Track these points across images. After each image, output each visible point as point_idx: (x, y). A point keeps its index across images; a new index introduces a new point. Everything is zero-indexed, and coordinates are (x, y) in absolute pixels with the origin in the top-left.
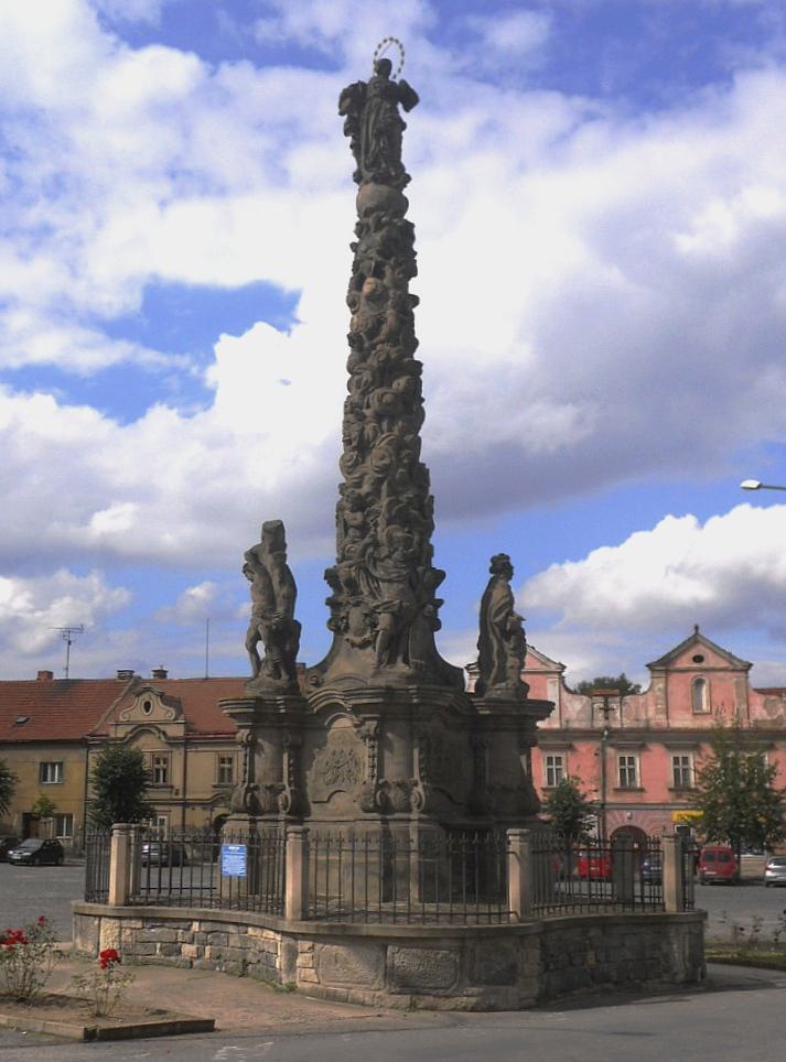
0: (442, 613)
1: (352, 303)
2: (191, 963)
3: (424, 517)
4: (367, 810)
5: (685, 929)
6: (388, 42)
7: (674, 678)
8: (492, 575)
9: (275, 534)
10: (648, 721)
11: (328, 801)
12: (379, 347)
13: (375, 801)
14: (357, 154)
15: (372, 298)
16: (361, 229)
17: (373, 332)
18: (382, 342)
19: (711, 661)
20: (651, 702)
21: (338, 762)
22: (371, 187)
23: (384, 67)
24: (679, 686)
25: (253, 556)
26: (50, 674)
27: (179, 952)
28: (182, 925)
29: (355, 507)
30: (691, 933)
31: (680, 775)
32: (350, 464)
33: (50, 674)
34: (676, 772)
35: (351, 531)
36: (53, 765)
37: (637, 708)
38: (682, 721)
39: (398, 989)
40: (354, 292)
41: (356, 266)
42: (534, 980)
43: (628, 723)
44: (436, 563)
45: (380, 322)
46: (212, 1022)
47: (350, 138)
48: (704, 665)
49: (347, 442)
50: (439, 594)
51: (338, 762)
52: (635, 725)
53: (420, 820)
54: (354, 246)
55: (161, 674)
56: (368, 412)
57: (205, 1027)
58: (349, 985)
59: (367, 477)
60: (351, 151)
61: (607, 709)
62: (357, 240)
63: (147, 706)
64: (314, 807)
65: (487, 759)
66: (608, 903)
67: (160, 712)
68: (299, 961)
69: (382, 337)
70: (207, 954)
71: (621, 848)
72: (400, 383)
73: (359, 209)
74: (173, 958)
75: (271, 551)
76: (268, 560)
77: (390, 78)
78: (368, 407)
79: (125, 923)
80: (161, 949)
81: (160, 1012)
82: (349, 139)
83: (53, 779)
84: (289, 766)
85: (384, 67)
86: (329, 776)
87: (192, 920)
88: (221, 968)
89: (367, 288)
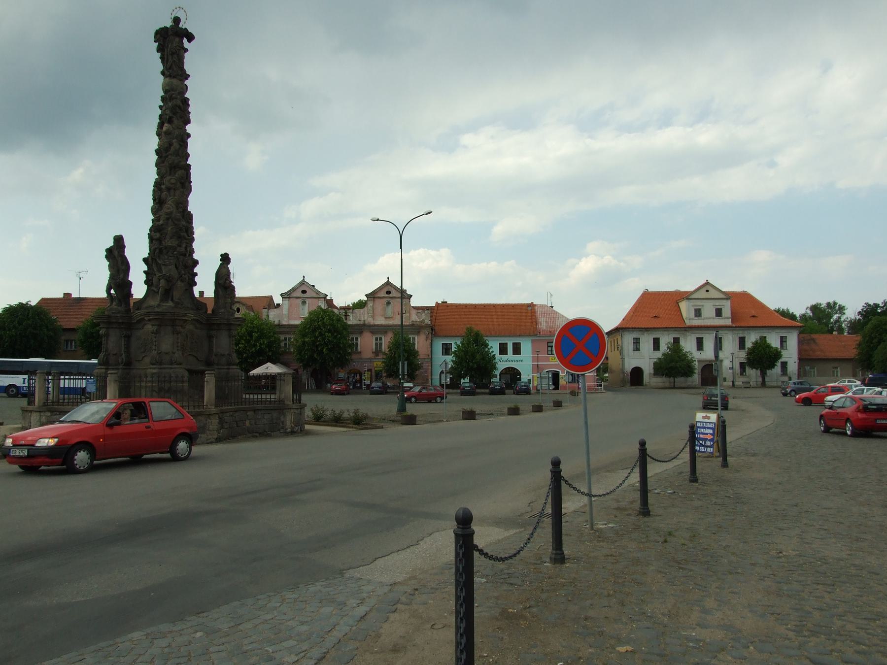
0: (197, 279)
4: (153, 364)
7: (378, 301)
9: (119, 241)
14: (163, 62)
15: (168, 133)
16: (163, 99)
17: (167, 149)
22: (167, 79)
23: (177, 20)
31: (379, 345)
34: (376, 344)
36: (71, 341)
38: (380, 321)
41: (161, 117)
44: (195, 256)
45: (171, 145)
48: (391, 295)
49: (154, 200)
50: (196, 270)
54: (161, 107)
56: (163, 187)
72: (180, 173)
76: (116, 253)
85: (177, 20)
89: (164, 129)
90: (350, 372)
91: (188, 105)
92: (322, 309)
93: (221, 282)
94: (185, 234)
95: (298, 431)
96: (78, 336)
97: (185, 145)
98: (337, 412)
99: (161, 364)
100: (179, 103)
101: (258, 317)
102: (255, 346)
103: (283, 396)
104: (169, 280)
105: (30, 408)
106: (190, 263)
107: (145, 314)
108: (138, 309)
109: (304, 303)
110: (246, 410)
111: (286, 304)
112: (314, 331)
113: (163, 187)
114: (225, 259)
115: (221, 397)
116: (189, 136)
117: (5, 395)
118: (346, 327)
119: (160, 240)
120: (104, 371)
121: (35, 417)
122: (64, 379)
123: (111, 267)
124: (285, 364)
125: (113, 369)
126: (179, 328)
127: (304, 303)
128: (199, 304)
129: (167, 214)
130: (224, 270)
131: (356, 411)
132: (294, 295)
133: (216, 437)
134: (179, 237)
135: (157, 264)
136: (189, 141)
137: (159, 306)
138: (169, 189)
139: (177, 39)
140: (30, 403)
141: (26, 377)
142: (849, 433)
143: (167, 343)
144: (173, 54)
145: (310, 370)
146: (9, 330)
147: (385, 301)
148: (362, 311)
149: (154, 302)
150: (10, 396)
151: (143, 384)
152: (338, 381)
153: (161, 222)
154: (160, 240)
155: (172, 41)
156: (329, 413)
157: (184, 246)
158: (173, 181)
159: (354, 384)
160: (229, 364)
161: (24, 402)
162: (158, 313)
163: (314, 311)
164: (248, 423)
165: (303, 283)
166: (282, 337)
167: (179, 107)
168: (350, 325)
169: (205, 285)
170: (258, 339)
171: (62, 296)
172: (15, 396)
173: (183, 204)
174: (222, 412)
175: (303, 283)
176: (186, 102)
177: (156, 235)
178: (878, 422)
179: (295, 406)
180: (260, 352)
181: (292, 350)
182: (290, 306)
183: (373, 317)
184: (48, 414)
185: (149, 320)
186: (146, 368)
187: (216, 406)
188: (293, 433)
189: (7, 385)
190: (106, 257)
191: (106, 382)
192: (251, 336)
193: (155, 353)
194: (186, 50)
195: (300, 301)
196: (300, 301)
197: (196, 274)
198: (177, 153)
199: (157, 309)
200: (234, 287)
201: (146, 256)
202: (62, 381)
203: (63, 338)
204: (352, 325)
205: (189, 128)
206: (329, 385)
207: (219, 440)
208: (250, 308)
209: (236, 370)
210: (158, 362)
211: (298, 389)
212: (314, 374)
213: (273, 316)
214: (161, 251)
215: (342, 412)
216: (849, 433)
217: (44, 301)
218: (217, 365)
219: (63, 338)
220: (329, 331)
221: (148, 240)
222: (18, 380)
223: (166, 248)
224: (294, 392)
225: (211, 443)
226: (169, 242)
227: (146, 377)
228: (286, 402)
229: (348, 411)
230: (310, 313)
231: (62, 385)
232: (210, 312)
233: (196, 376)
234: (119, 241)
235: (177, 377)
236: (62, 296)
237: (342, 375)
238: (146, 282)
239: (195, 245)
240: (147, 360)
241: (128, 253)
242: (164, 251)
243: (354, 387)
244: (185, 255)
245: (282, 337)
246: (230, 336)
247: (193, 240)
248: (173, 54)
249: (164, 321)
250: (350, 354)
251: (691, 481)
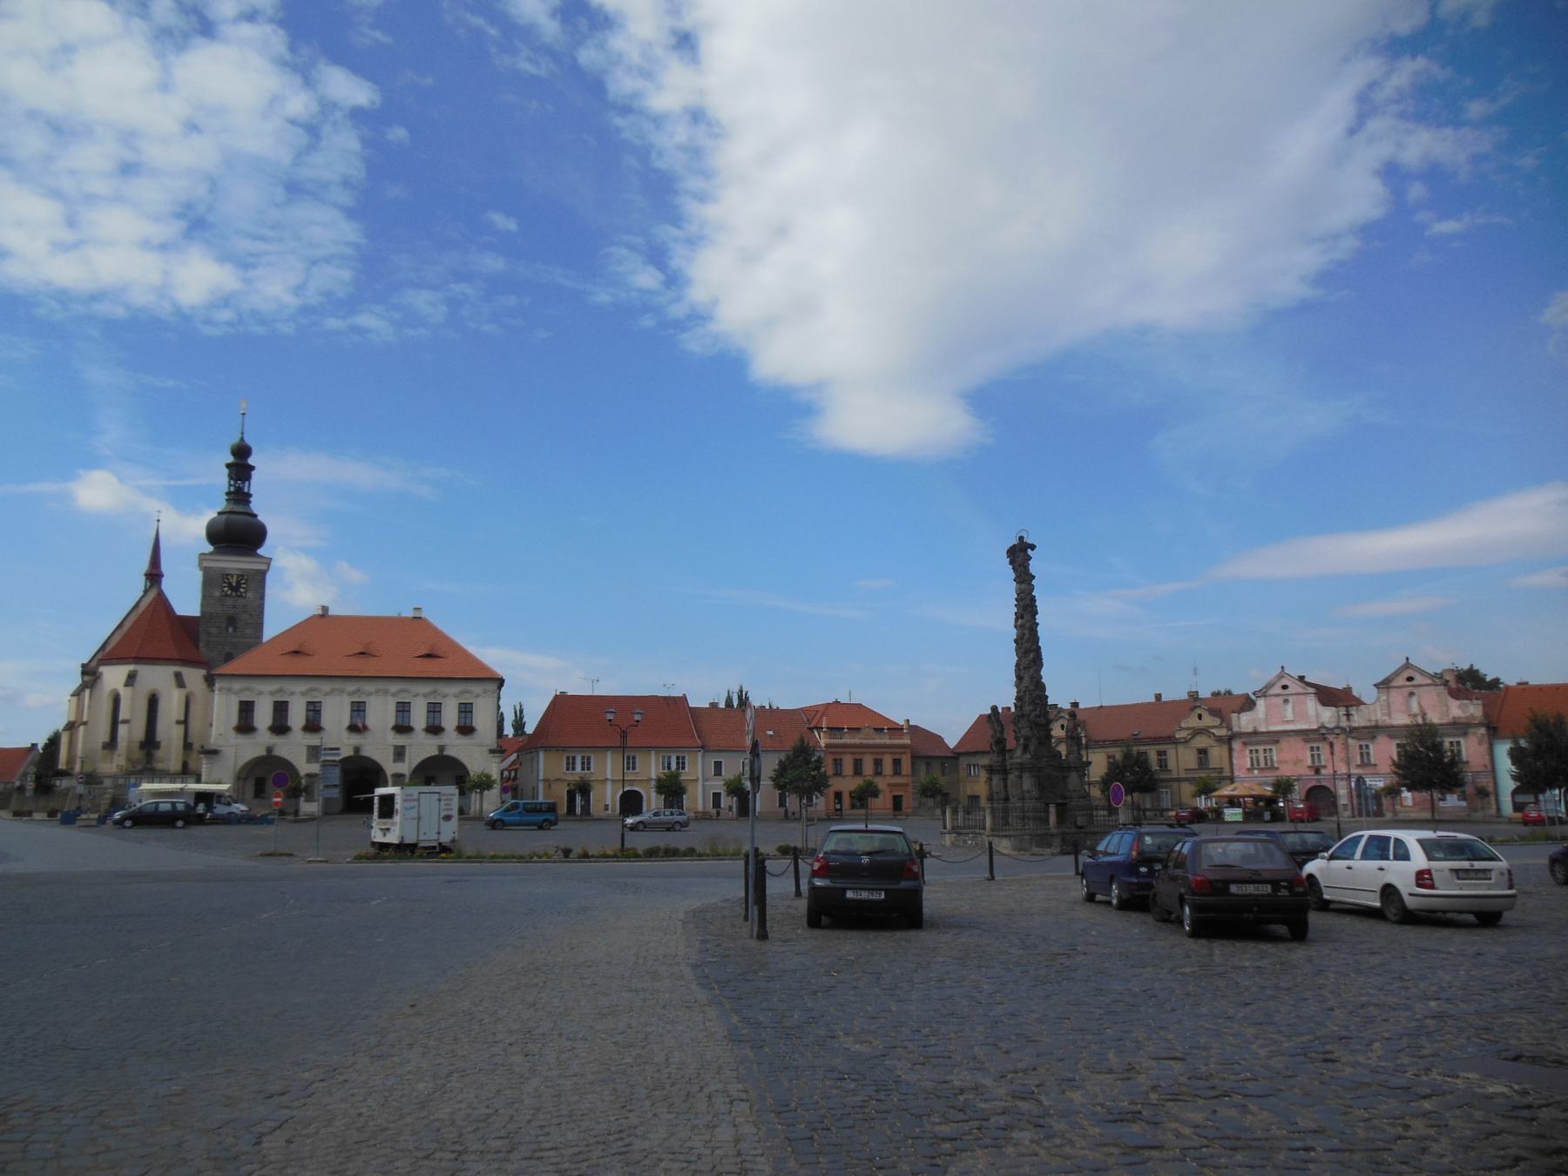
7: (1394, 693)
19: (1419, 679)
23: (1021, 538)
24: (1397, 698)
29: (46, 747)
43: (1363, 723)
55: (1075, 705)
61: (1348, 715)
63: (1200, 717)
66: (264, 1134)
67: (1208, 720)
72: (1032, 656)
85: (1021, 538)
142: (1115, 901)
147: (1406, 691)
155: (1019, 554)
178: (850, 895)
183: (1389, 715)
195: (1280, 700)
196: (1280, 700)
216: (1115, 901)
251: (1299, 933)
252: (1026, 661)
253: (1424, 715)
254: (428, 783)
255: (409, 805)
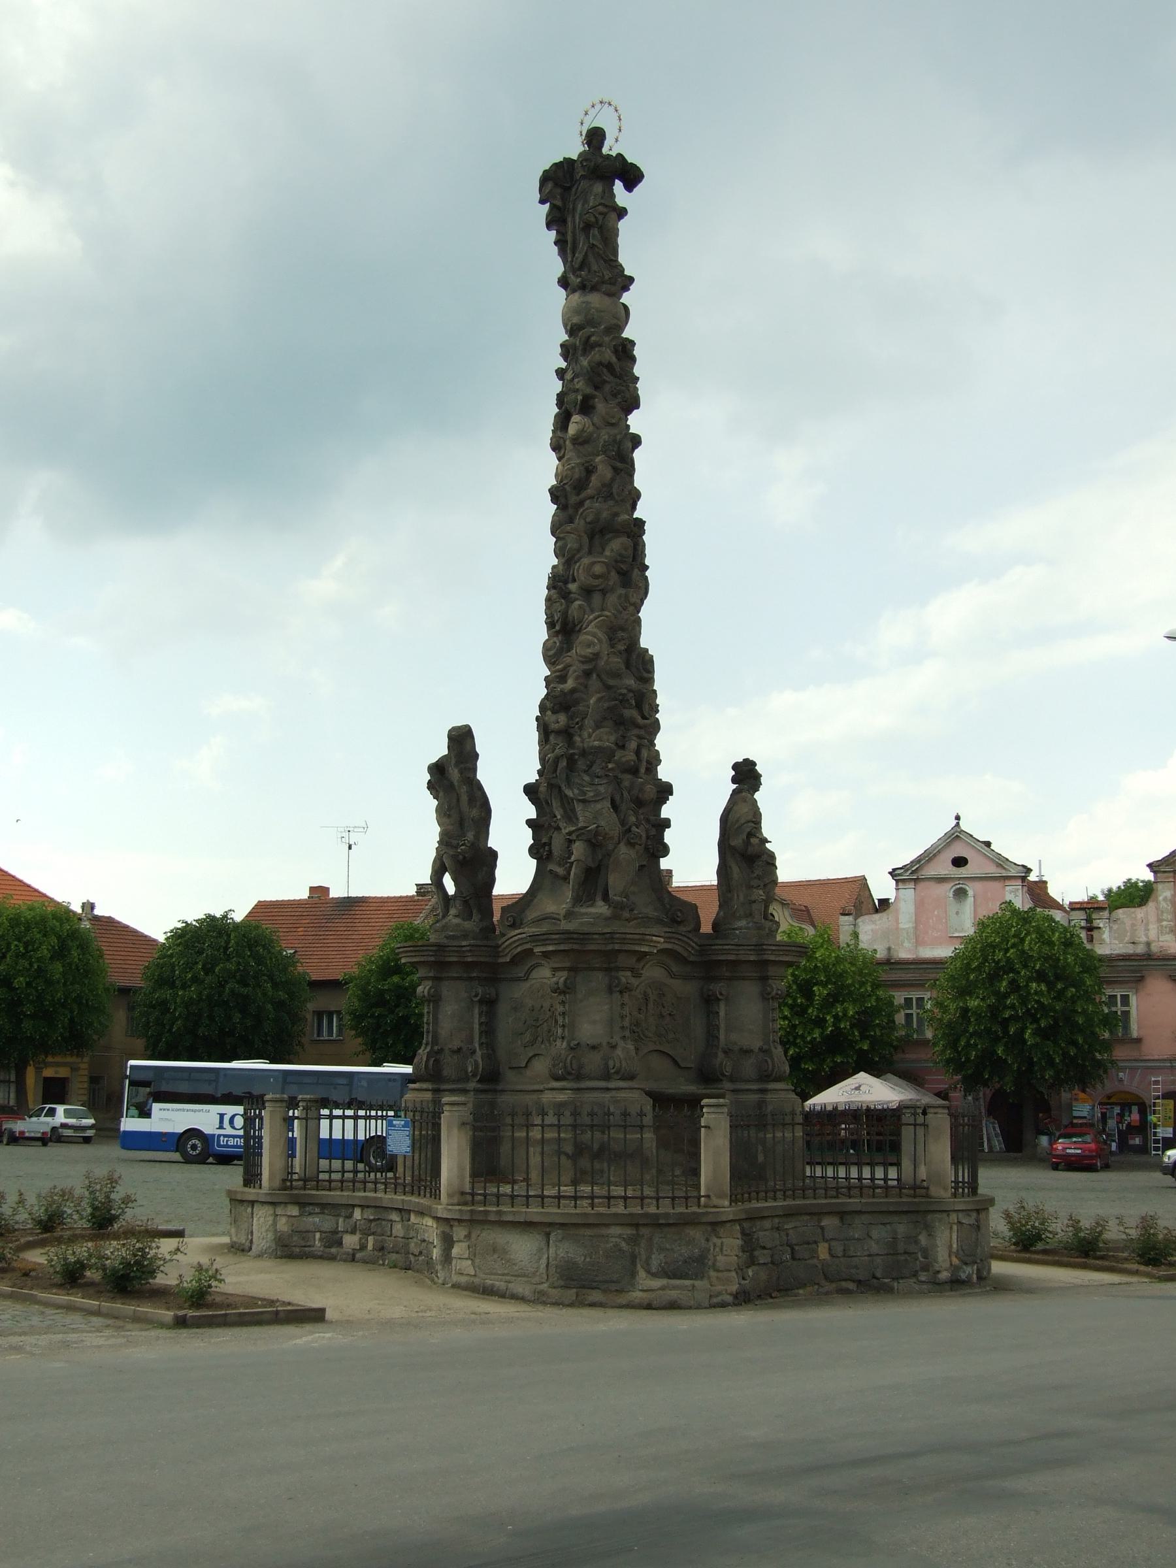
0: (669, 836)
1: (556, 447)
2: (354, 1255)
3: (644, 718)
4: (557, 1079)
5: (954, 1217)
6: (598, 106)
8: (735, 786)
9: (462, 742)
10: (1148, 944)
11: (526, 1066)
12: (587, 503)
13: (565, 1067)
14: (562, 253)
15: (580, 441)
16: (567, 351)
17: (580, 485)
18: (592, 498)
20: (1152, 918)
21: (537, 1020)
23: (595, 137)
25: (438, 769)
26: (326, 890)
27: (340, 1243)
28: (343, 1212)
30: (959, 1222)
32: (552, 653)
33: (324, 890)
35: (552, 738)
36: (330, 1015)
37: (1133, 925)
39: (562, 1283)
40: (559, 434)
41: (561, 399)
42: (733, 1274)
45: (589, 471)
46: (323, 1310)
47: (554, 232)
49: (550, 624)
50: (666, 812)
51: (537, 1020)
52: (1130, 950)
53: (476, 1091)
54: (560, 373)
56: (573, 587)
57: (315, 1316)
58: (508, 1278)
59: (572, 669)
60: (556, 249)
62: (564, 365)
64: (510, 1075)
65: (722, 1013)
68: (455, 1251)
69: (589, 492)
70: (370, 1246)
71: (912, 1121)
72: (617, 545)
73: (565, 326)
74: (333, 1250)
75: (456, 765)
76: (454, 774)
77: (605, 151)
78: (574, 580)
79: (279, 1211)
80: (321, 1240)
81: (289, 1304)
82: (553, 234)
83: (330, 1032)
84: (481, 1024)
85: (595, 137)
86: (528, 1037)
87: (354, 1206)
88: (384, 1260)
89: (572, 429)
90: (1107, 1102)
91: (633, 359)
92: (1015, 912)
93: (737, 842)
94: (633, 713)
95: (969, 1279)
96: (346, 1002)
97: (626, 468)
98: (1086, 1223)
99: (579, 1077)
100: (609, 356)
101: (829, 941)
102: (820, 1023)
103: (923, 1172)
104: (595, 842)
105: (251, 1193)
106: (650, 792)
107: (534, 938)
108: (513, 926)
109: (960, 894)
110: (817, 1213)
111: (906, 901)
112: (994, 977)
113: (573, 587)
114: (746, 776)
115: (747, 1173)
116: (636, 441)
117: (177, 1156)
118: (1091, 963)
119: (567, 734)
120: (428, 1096)
121: (263, 1224)
122: (331, 1117)
123: (443, 813)
124: (910, 1077)
125: (452, 1091)
126: (625, 977)
127: (960, 894)
128: (676, 908)
129: (586, 660)
130: (743, 809)
131: (1147, 1223)
132: (931, 870)
133: (734, 1288)
134: (621, 723)
135: (563, 798)
136: (638, 455)
137: (569, 915)
138: (587, 592)
139: (598, 188)
140: (252, 1178)
141: (240, 1109)
143: (593, 1019)
144: (587, 227)
145: (985, 1093)
146: (184, 987)
148: (1140, 913)
149: (556, 905)
150: (188, 1160)
151: (536, 1134)
152: (1072, 1130)
153: (570, 684)
154: (567, 734)
155: (585, 196)
156: (1059, 1229)
157: (633, 745)
158: (598, 569)
159: (1123, 1137)
160: (766, 1077)
161: (232, 1176)
162: (568, 936)
163: (993, 919)
164: (823, 1251)
165: (956, 835)
166: (899, 997)
167: (609, 366)
168: (1102, 959)
169: (692, 858)
170: (833, 999)
171: (304, 895)
172: (201, 1160)
173: (625, 630)
174: (753, 1218)
175: (956, 835)
176: (626, 351)
177: (559, 719)
179: (961, 1204)
180: (836, 1042)
181: (929, 1034)
182: (920, 905)
184: (294, 1211)
185: (546, 955)
186: (538, 1087)
187: (734, 1200)
188: (956, 1284)
189: (180, 1129)
190: (431, 786)
191: (437, 1127)
192: (808, 994)
193: (561, 1046)
194: (622, 213)
195: (947, 890)
196: (947, 890)
197: (667, 823)
198: (606, 492)
199: (565, 925)
200: (772, 856)
201: (533, 777)
202: (324, 1123)
203: (310, 1006)
204: (1110, 960)
205: (636, 422)
206: (1044, 1140)
207: (743, 1299)
208: (804, 914)
209: (781, 1094)
210: (570, 1073)
211: (967, 1152)
212: (998, 1107)
213: (870, 936)
214: (571, 761)
215: (1101, 1224)
217: (262, 908)
218: (732, 1079)
219: (310, 1006)
220: (1041, 976)
221: (535, 736)
222: (204, 1118)
223: (583, 753)
224: (955, 1160)
225: (723, 1305)
226: (595, 737)
227: (544, 1114)
228: (934, 1191)
229: (1120, 1220)
230: (982, 925)
231: (324, 1134)
232: (706, 928)
233: (677, 1113)
234: (462, 742)
235: (625, 1114)
236: (304, 895)
237: (1083, 1109)
238: (534, 851)
239: (661, 742)
240: (540, 1067)
241: (484, 774)
242: (581, 764)
243: (1123, 1146)
244: (634, 771)
245: (899, 997)
246: (765, 996)
247: (655, 727)
248: (587, 227)
249: (587, 956)
250: (1107, 1046)
252: (590, 566)
253: (1148, 944)
254: (1147, 1264)
255: (416, 1192)
